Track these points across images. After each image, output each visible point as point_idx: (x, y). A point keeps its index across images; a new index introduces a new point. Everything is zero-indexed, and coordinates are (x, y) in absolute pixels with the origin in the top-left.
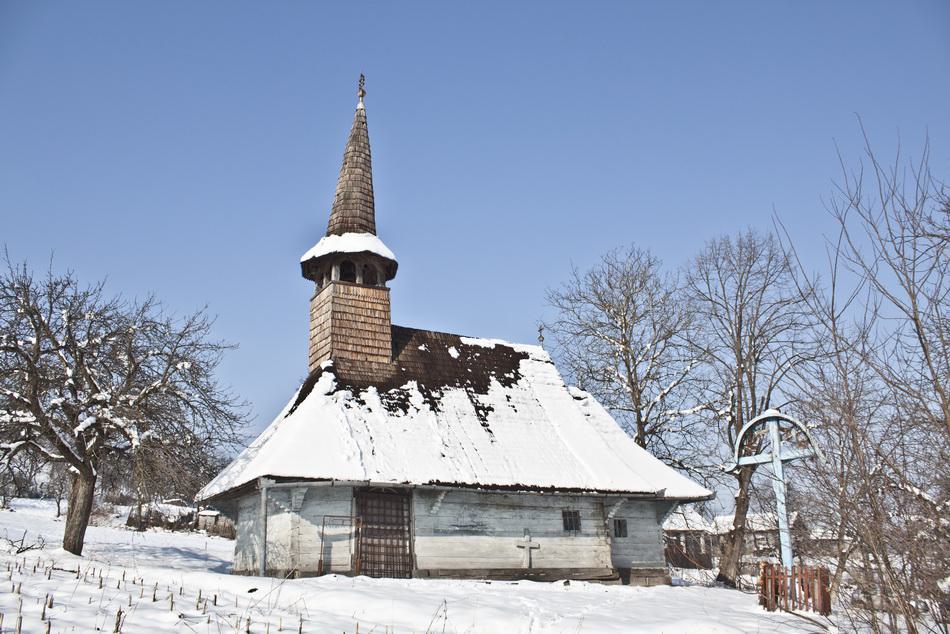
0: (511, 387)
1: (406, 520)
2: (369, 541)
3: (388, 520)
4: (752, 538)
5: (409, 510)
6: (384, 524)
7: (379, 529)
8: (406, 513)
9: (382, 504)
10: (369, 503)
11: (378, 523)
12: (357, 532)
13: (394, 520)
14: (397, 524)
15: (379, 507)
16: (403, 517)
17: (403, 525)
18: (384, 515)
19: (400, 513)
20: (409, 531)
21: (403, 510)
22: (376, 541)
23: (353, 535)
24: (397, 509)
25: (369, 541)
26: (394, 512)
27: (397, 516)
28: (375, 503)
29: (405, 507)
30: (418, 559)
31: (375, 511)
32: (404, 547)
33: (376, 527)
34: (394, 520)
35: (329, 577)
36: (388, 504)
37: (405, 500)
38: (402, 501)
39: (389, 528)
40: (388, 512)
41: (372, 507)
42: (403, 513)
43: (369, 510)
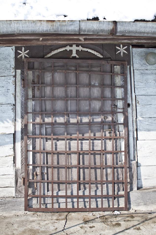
0: (4, 123)
1: (120, 104)
2: (49, 145)
3: (84, 105)
4: (122, 193)
5: (124, 86)
6: (79, 113)
7: (67, 124)
8: (119, 92)
9: (72, 78)
10: (48, 78)
11: (66, 113)
12: (25, 130)
13: (97, 105)
14: (102, 112)
15: (66, 84)
16: (114, 98)
17: (113, 113)
18: (77, 97)
19: (108, 93)
20: (126, 124)
21: (113, 86)
22: (61, 145)
23: (19, 136)
24: (102, 85)
25: (49, 145)
26: (96, 92)
27: (103, 98)
28: (59, 77)
29: (118, 80)
30: (143, 171)
31: (59, 91)
32: (115, 152)
33: (61, 120)
34: (97, 105)
35: (62, 230)
36: (84, 78)
37: (117, 68)
38: (112, 71)
39: (85, 120)
40: (84, 91)
41: (53, 84)
42: (113, 93)
43: (48, 90)
